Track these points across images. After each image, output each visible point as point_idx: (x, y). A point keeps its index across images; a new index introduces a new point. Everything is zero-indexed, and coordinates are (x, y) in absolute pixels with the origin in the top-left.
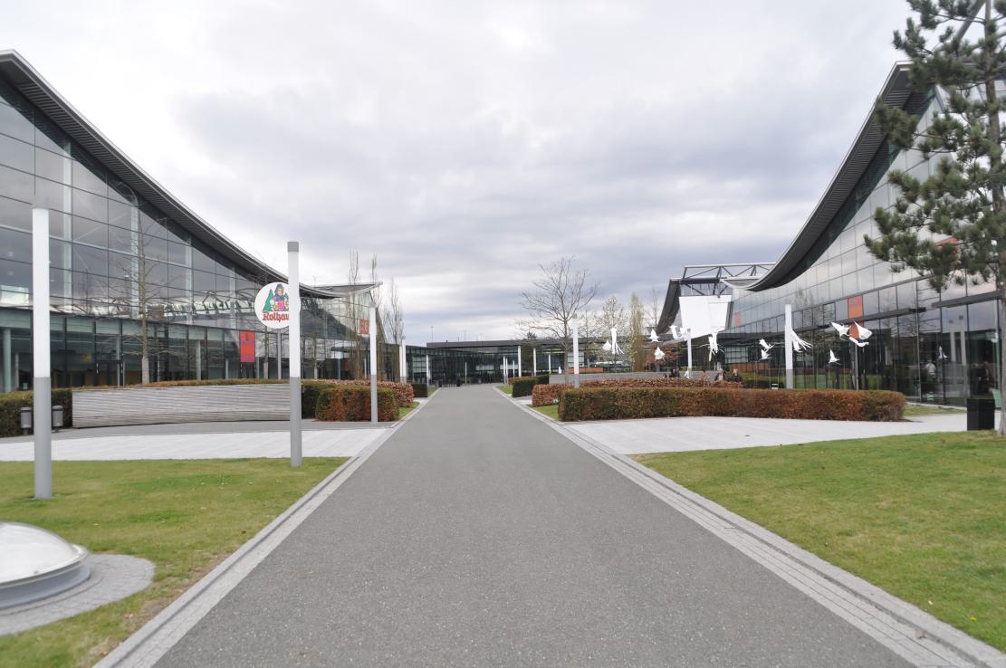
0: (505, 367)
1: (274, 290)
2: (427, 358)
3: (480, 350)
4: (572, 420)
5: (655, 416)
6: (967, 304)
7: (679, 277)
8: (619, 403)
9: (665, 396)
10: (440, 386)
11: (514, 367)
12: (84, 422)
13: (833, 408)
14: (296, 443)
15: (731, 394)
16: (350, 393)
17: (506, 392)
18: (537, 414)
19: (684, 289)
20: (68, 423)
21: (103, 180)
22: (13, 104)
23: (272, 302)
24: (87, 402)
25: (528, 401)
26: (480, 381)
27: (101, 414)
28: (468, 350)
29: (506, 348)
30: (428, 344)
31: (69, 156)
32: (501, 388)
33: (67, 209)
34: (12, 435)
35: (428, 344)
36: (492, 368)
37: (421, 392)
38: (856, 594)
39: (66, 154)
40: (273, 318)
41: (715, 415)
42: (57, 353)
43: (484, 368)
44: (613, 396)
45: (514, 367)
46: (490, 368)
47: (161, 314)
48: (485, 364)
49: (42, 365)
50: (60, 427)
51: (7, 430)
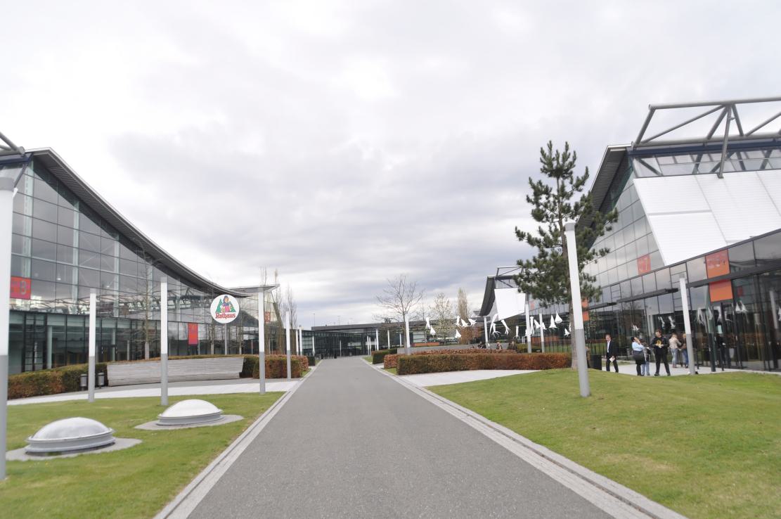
0: (369, 344)
1: (222, 300)
2: (313, 338)
3: (351, 332)
4: (404, 374)
5: (451, 371)
6: (657, 295)
7: (494, 275)
8: (430, 364)
9: (456, 359)
10: (322, 358)
11: (373, 343)
12: (115, 382)
13: (550, 363)
14: (263, 387)
15: (493, 356)
16: (273, 362)
17: (369, 361)
18: (386, 373)
19: (498, 283)
20: (106, 384)
21: (98, 224)
22: (44, 180)
23: (221, 307)
24: (116, 370)
25: (382, 366)
26: (351, 354)
27: (124, 377)
28: (342, 331)
29: (368, 330)
30: (312, 328)
31: (78, 210)
32: (366, 359)
33: (76, 244)
34: (74, 391)
35: (312, 328)
36: (359, 344)
37: (312, 363)
38: (573, 472)
39: (75, 209)
40: (221, 317)
41: (485, 369)
42: (99, 342)
43: (353, 344)
44: (427, 359)
45: (373, 343)
46: (357, 345)
47: (103, 313)
48: (354, 342)
49: (92, 351)
50: (102, 386)
51: (72, 388)
